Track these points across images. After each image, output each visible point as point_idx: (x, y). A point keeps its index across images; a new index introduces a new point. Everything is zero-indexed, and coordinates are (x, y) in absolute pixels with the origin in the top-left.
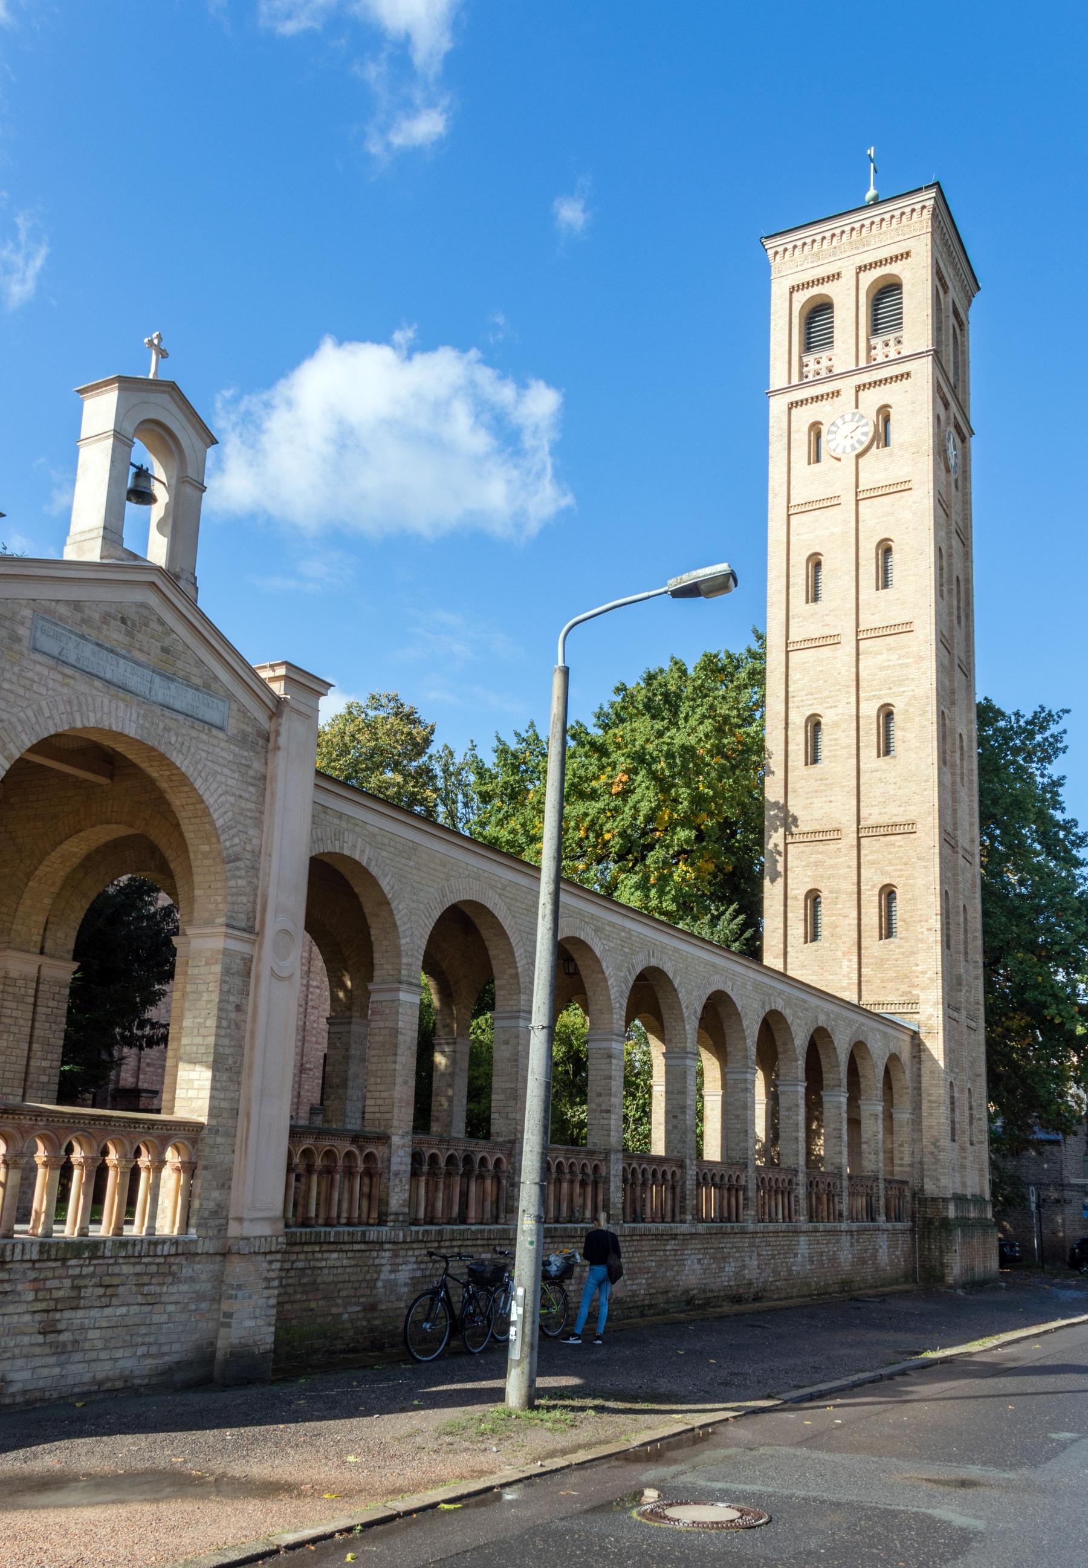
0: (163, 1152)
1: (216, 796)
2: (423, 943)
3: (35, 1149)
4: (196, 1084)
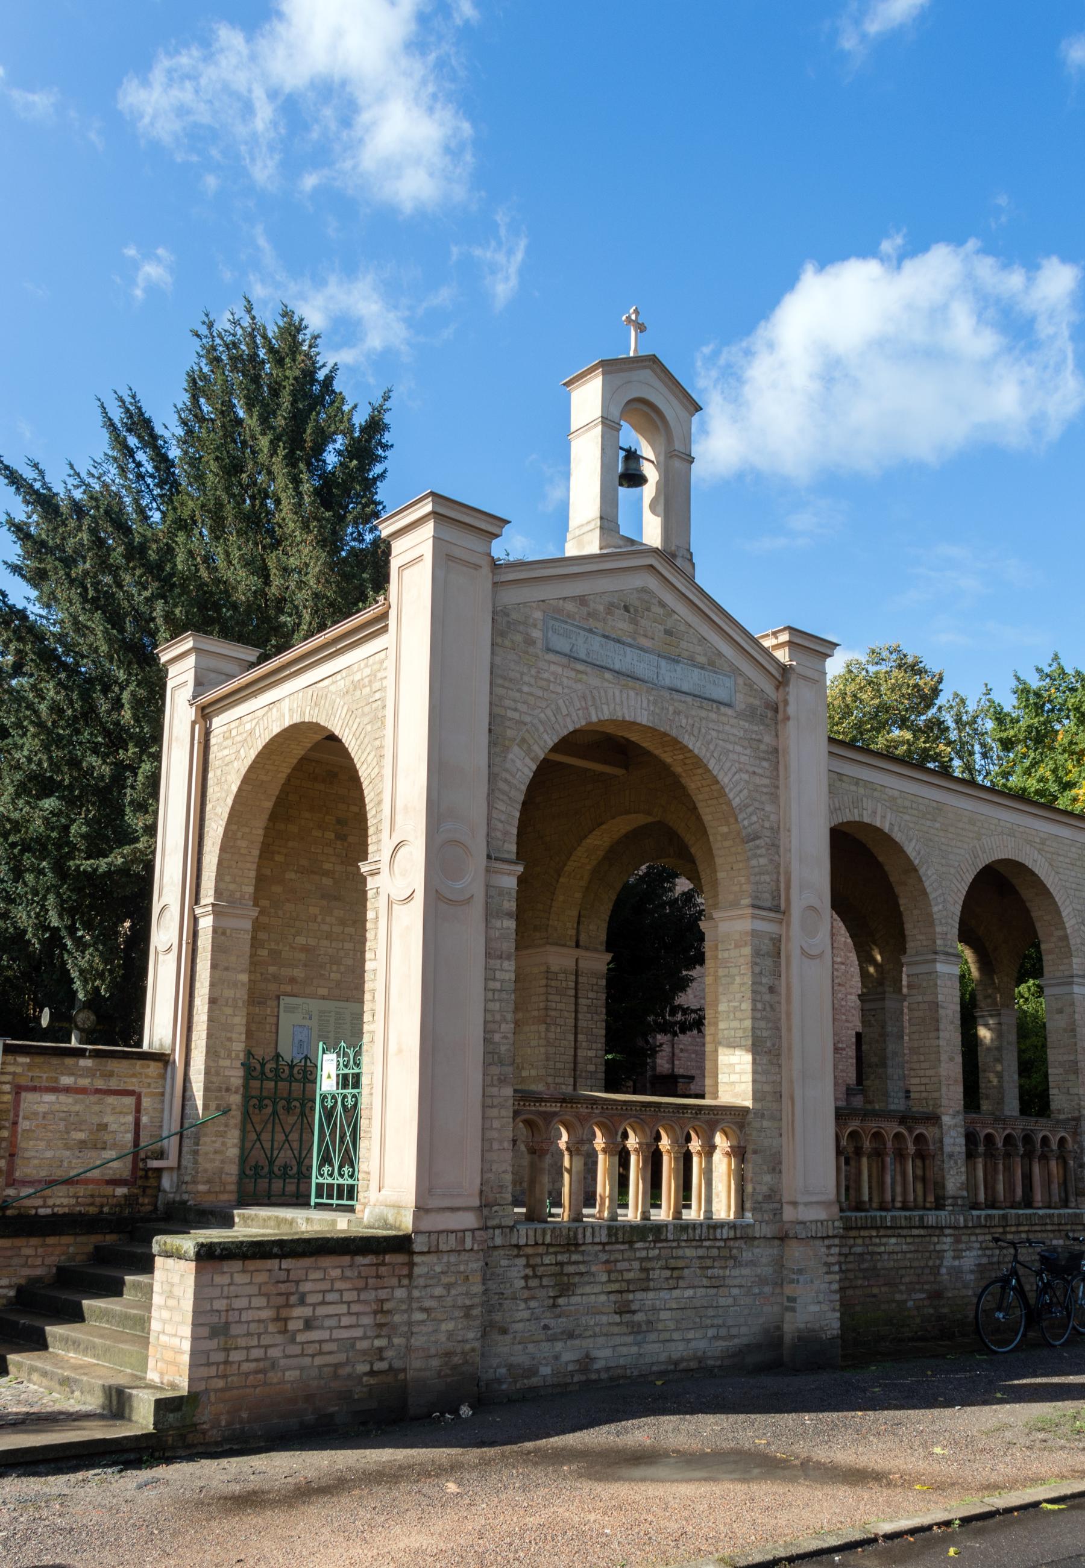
0: (712, 1137)
1: (730, 775)
2: (957, 909)
3: (594, 1135)
4: (738, 1068)
